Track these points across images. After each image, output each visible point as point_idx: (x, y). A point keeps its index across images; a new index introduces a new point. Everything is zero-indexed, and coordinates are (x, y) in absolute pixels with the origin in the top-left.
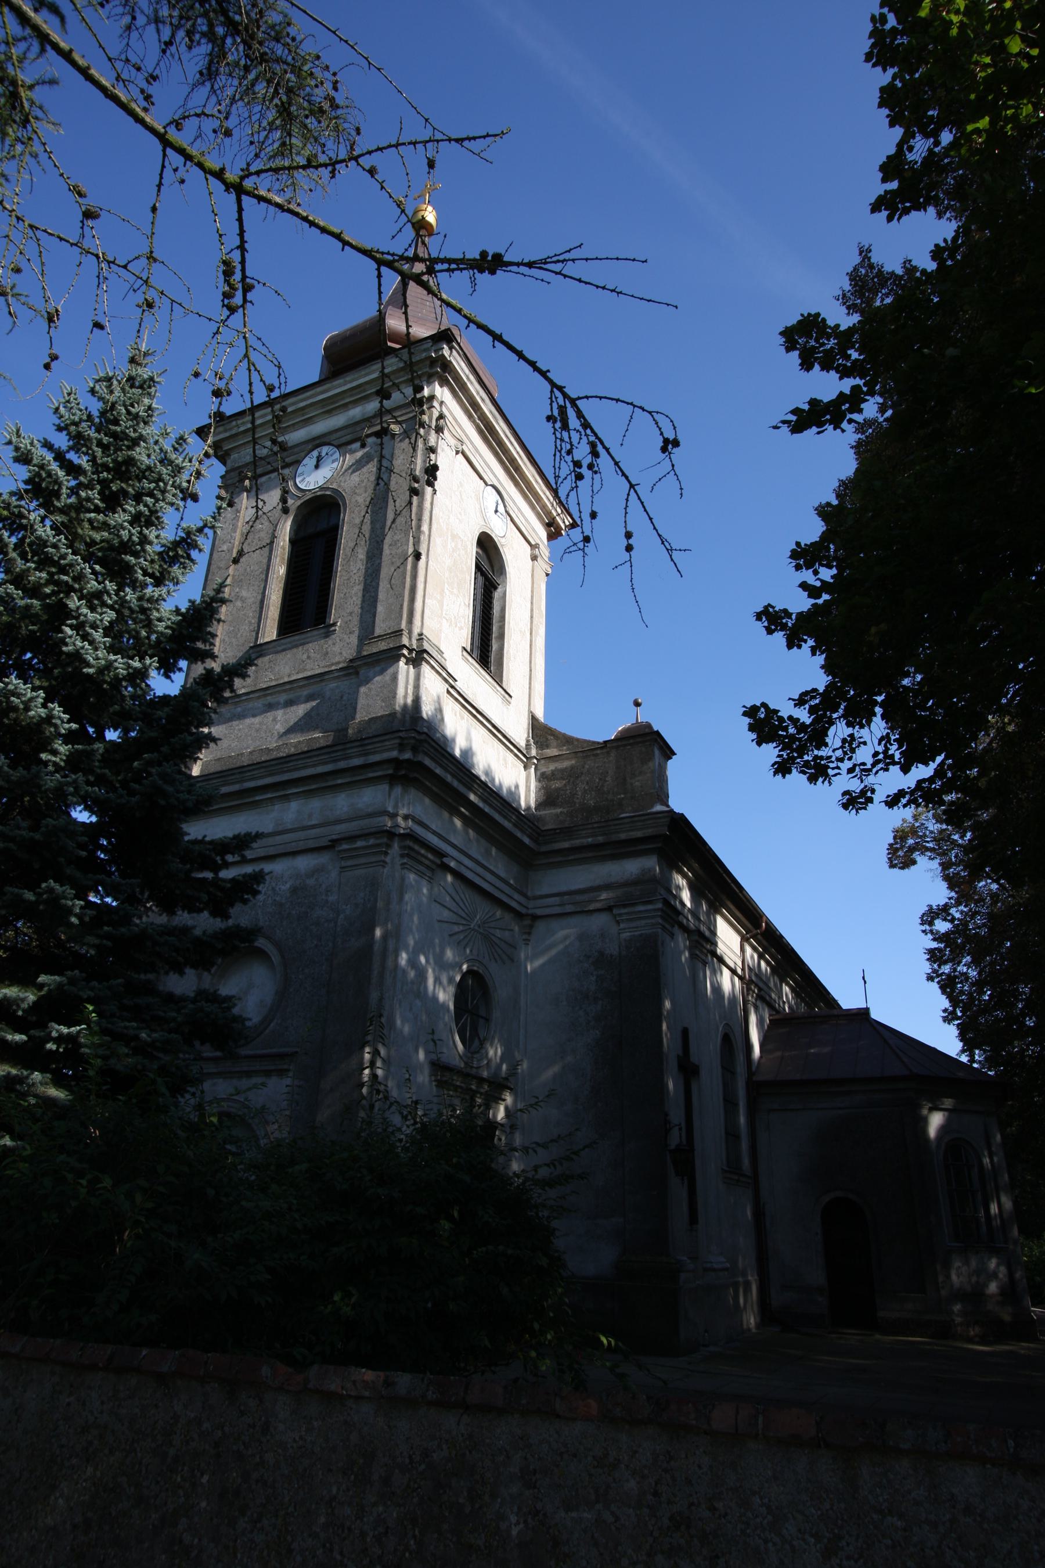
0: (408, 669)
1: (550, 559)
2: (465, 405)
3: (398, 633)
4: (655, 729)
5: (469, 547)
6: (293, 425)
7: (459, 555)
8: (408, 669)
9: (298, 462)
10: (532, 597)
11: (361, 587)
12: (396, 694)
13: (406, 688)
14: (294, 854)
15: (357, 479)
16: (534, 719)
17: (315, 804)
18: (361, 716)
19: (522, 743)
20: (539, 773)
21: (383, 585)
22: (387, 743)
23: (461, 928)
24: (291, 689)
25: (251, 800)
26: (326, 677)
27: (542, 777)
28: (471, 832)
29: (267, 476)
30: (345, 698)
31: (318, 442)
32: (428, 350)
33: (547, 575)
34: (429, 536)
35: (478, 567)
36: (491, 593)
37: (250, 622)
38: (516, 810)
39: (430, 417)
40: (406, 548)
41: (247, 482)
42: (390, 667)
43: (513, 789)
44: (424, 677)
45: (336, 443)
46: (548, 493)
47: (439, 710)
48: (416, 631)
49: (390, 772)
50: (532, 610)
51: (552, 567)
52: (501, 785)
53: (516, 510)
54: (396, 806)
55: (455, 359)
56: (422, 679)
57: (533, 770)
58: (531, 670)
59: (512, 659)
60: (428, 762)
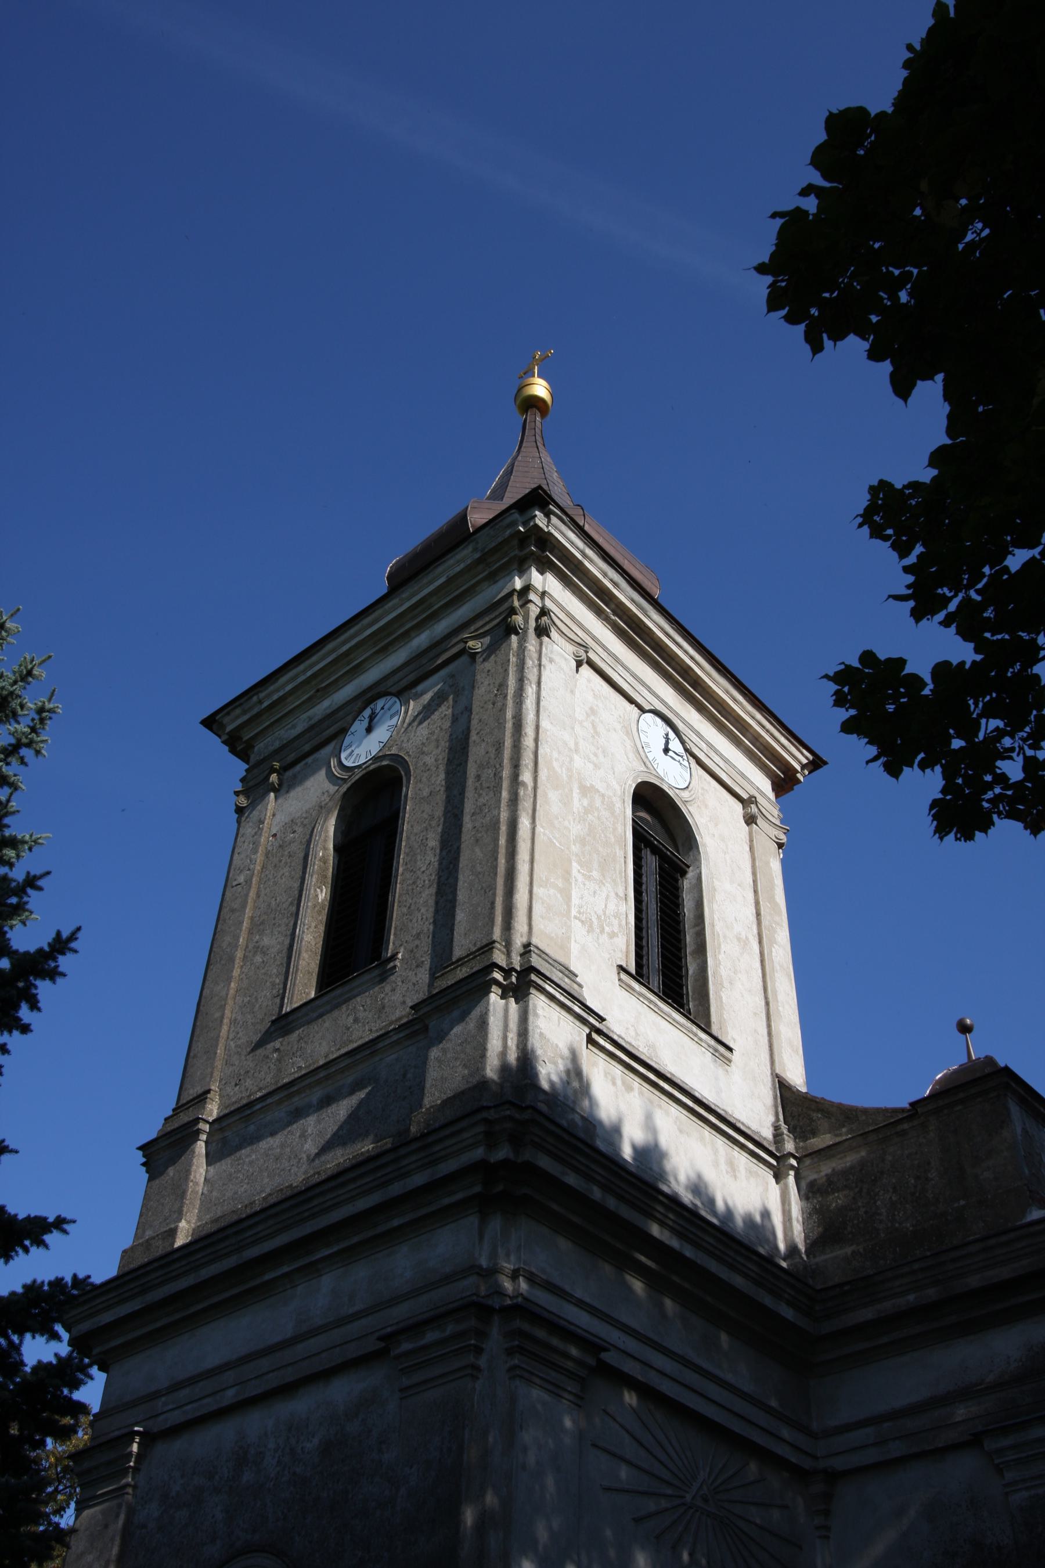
0: (507, 1004)
1: (782, 822)
2: (587, 595)
3: (489, 946)
4: (1002, 1064)
5: (618, 805)
6: (337, 680)
7: (599, 818)
8: (507, 1004)
9: (344, 731)
10: (755, 882)
11: (433, 890)
12: (485, 1049)
13: (505, 1038)
14: (326, 1375)
15: (425, 732)
16: (783, 1088)
17: (361, 1273)
18: (433, 1097)
19: (766, 1133)
20: (803, 1184)
21: (464, 879)
22: (465, 1135)
23: (664, 1503)
24: (327, 1078)
25: (258, 1281)
26: (381, 1045)
27: (809, 1192)
28: (668, 1303)
29: (303, 762)
30: (409, 1076)
31: (369, 695)
32: (514, 524)
33: (780, 846)
34: (535, 788)
35: (641, 840)
36: (677, 881)
37: (273, 984)
38: (768, 1262)
39: (527, 618)
40: (495, 812)
41: (274, 778)
42: (476, 1006)
43: (758, 1218)
44: (536, 1015)
45: (393, 690)
46: (759, 716)
47: (575, 1071)
48: (518, 941)
49: (478, 1189)
50: (757, 904)
51: (787, 832)
52: (729, 1213)
53: (704, 746)
54: (493, 1256)
55: (556, 528)
56: (531, 1018)
57: (791, 1179)
58: (767, 1004)
59: (726, 984)
60: (544, 1162)
